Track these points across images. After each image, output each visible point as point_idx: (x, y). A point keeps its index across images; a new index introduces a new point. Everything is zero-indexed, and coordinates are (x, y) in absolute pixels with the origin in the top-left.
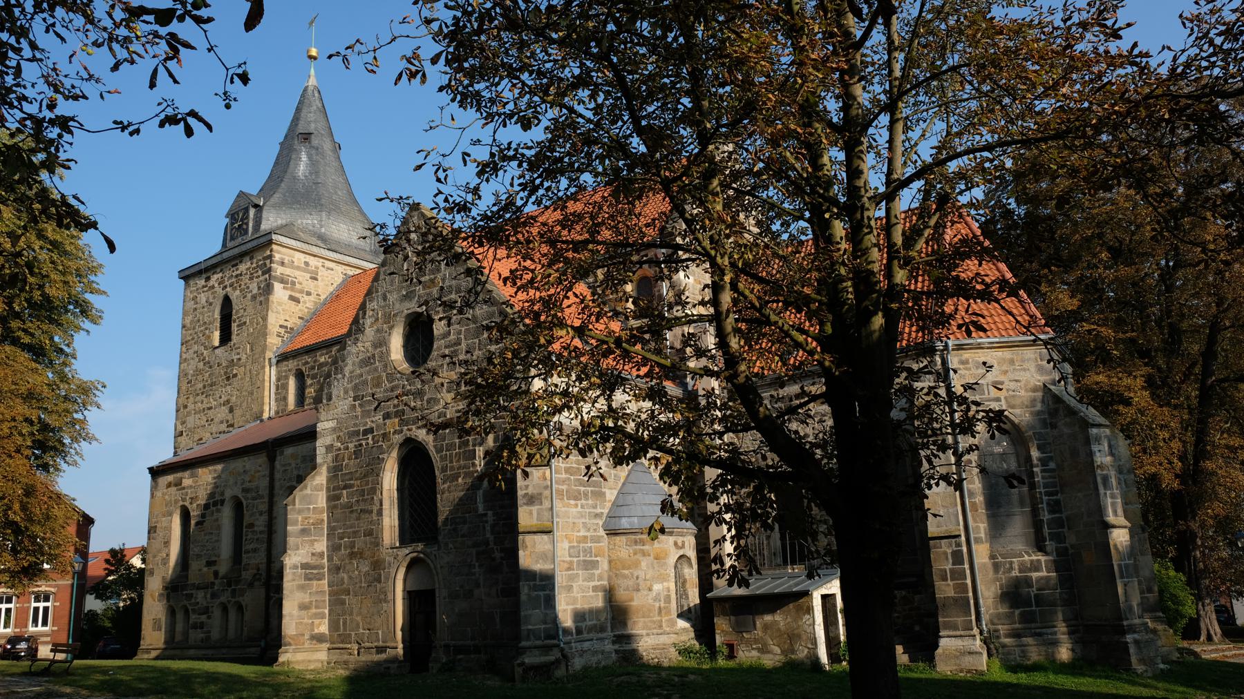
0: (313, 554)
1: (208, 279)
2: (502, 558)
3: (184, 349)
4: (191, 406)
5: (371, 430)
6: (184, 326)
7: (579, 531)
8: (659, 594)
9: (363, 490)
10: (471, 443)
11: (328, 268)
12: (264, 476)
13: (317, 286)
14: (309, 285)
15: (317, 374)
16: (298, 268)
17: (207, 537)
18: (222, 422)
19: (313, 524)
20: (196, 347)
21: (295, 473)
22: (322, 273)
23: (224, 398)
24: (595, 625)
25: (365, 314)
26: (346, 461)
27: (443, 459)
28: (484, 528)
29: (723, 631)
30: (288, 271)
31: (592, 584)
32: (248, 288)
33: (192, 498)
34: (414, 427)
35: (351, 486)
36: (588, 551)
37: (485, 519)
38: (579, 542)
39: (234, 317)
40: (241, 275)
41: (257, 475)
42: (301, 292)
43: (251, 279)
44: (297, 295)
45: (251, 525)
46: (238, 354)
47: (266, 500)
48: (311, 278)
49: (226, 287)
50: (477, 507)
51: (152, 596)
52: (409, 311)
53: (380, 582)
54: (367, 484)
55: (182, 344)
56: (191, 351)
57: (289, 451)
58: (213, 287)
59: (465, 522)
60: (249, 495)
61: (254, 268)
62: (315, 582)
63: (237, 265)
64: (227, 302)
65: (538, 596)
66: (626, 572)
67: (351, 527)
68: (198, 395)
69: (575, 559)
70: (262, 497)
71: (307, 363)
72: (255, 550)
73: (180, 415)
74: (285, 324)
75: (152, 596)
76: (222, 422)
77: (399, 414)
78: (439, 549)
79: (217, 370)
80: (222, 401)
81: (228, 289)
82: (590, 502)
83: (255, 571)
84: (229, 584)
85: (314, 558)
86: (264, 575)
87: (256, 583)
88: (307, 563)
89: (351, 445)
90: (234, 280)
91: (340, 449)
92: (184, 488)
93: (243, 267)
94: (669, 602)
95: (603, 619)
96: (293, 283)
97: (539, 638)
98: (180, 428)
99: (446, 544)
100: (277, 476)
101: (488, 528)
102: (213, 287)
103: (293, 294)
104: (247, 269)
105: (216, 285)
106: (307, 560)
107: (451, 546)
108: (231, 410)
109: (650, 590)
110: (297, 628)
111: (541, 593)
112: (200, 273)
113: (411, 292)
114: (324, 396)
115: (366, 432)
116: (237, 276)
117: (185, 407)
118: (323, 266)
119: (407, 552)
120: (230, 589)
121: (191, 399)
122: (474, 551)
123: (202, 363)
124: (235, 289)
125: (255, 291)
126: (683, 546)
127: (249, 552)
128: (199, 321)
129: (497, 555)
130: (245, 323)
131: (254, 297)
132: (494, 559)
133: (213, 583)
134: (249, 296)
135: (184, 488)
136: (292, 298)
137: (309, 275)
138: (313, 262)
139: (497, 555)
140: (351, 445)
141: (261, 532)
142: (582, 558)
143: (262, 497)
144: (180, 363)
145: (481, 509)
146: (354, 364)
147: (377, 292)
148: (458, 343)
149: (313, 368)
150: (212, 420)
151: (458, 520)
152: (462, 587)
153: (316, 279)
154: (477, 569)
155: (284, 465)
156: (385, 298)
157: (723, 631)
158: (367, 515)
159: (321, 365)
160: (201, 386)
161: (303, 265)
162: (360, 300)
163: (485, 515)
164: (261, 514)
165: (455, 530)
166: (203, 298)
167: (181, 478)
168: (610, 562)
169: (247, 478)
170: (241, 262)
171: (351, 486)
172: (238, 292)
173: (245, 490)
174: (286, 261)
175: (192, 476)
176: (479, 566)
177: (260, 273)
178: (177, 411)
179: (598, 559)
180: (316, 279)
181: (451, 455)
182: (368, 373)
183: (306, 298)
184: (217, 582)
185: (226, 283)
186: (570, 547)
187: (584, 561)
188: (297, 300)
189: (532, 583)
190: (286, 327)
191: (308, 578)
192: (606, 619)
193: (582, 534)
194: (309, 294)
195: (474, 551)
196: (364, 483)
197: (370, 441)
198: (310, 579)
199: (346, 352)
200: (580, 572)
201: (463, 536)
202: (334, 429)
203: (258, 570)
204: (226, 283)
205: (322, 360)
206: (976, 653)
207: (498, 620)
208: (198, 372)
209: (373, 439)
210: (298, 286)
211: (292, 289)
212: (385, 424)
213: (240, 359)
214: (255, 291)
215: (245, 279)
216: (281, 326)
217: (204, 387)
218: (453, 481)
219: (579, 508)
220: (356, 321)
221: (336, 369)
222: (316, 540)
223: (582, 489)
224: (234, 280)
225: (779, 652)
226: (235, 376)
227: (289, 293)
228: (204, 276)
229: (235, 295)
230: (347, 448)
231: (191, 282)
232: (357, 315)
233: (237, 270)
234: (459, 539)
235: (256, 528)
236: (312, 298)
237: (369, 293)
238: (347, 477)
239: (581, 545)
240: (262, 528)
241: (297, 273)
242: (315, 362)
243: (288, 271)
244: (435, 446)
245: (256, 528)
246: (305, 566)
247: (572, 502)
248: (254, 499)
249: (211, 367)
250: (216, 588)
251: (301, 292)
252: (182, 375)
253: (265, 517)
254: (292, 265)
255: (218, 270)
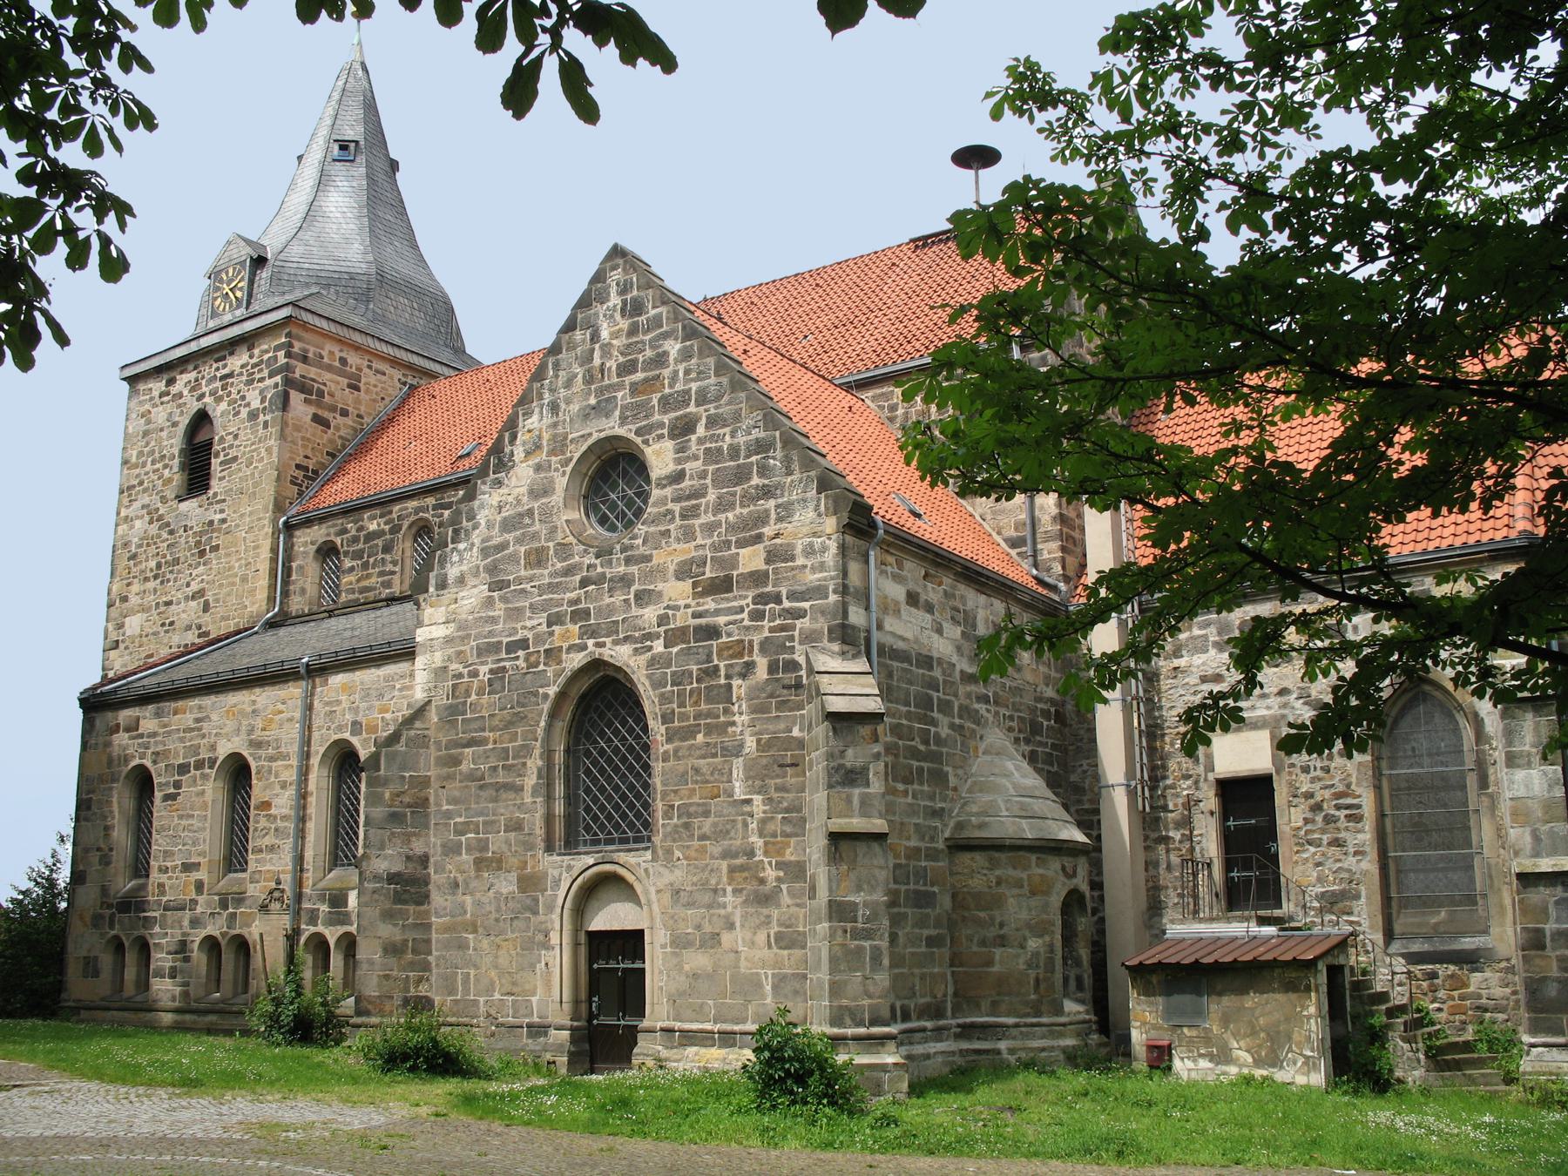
0: (408, 858)
1: (171, 382)
2: (778, 879)
3: (126, 501)
4: (134, 600)
5: (523, 644)
6: (125, 462)
7: (908, 839)
8: (1036, 954)
9: (506, 750)
10: (723, 673)
11: (377, 371)
12: (290, 720)
13: (358, 401)
14: (345, 397)
15: (362, 551)
16: (329, 368)
17: (184, 822)
18: (189, 628)
19: (409, 806)
20: (146, 500)
21: (349, 717)
22: (368, 378)
23: (195, 587)
24: (928, 1005)
25: (514, 438)
26: (474, 697)
27: (664, 699)
28: (745, 825)
29: (1144, 1023)
30: (312, 372)
31: (926, 932)
32: (243, 398)
33: (157, 754)
34: (608, 640)
35: (483, 742)
36: (921, 874)
37: (747, 809)
38: (908, 857)
39: (216, 447)
40: (231, 375)
41: (277, 718)
42: (333, 409)
43: (250, 382)
44: (326, 414)
45: (266, 805)
46: (222, 511)
47: (294, 762)
48: (350, 386)
49: (202, 396)
50: (733, 788)
51: (81, 918)
52: (603, 435)
53: (536, 913)
54: (514, 738)
55: (122, 492)
56: (137, 505)
57: (337, 680)
58: (180, 395)
59: (706, 814)
60: (261, 752)
61: (256, 365)
62: (411, 908)
63: (224, 358)
64: (202, 419)
65: (860, 949)
66: (982, 914)
67: (481, 814)
68: (146, 579)
69: (903, 888)
70: (286, 757)
71: (344, 531)
72: (272, 849)
73: (114, 612)
74: (305, 462)
75: (81, 918)
76: (189, 628)
77: (580, 615)
78: (653, 860)
79: (182, 538)
80: (189, 591)
81: (207, 399)
82: (926, 788)
83: (273, 885)
84: (224, 904)
85: (410, 865)
86: (289, 893)
87: (275, 906)
88: (398, 874)
89: (483, 669)
90: (218, 384)
91: (460, 676)
92: (141, 736)
93: (236, 362)
94: (1053, 971)
95: (939, 995)
96: (321, 394)
97: (860, 1024)
98: (113, 636)
99: (669, 852)
100: (318, 721)
101: (753, 826)
102: (180, 395)
103: (320, 412)
104: (242, 366)
105: (186, 393)
106: (398, 867)
107: (678, 854)
108: (206, 607)
109: (1022, 947)
110: (379, 985)
111: (867, 944)
112: (158, 371)
113: (607, 400)
114: (432, 582)
115: (512, 647)
116: (223, 378)
117: (125, 599)
118: (370, 367)
119: (591, 861)
120: (225, 914)
121: (135, 588)
122: (724, 865)
123: (156, 525)
124: (219, 400)
125: (256, 404)
126: (1074, 875)
127: (261, 851)
128: (153, 452)
129: (771, 874)
130: (235, 459)
131: (253, 416)
132: (762, 881)
133: (194, 902)
134: (244, 413)
135: (141, 736)
136: (317, 419)
137: (346, 381)
138: (354, 359)
139: (771, 874)
140: (483, 669)
141: (285, 818)
142: (912, 887)
143: (286, 757)
144: (117, 525)
145: (739, 792)
146: (490, 525)
147: (541, 397)
148: (699, 493)
149: (355, 540)
150: (172, 624)
151: (692, 809)
152: (698, 927)
153: (358, 389)
154: (729, 898)
155: (327, 704)
156: (554, 408)
157: (1144, 1023)
158: (512, 795)
159: (371, 536)
160: (153, 564)
161: (337, 364)
162: (507, 412)
163: (748, 802)
164: (284, 786)
165: (687, 826)
166: (160, 415)
167: (138, 719)
168: (954, 896)
169: (259, 723)
170: (232, 353)
171: (483, 742)
172: (223, 406)
173: (256, 745)
174: (310, 355)
175: (158, 715)
176: (735, 891)
177: (266, 373)
178: (110, 606)
179: (936, 889)
180: (358, 389)
181: (681, 694)
182: (519, 541)
183: (340, 420)
184: (201, 899)
185: (204, 389)
186: (896, 866)
187: (916, 892)
188: (325, 424)
189: (849, 925)
190: (306, 469)
191: (398, 898)
192: (945, 995)
193: (913, 843)
194: (344, 413)
195: (724, 865)
196: (507, 736)
197: (521, 663)
198: (405, 902)
199: (476, 503)
200: (909, 911)
201: (703, 838)
202: (449, 640)
203: (279, 883)
204: (204, 389)
205: (373, 526)
206: (218, 981)
207: (769, 988)
208: (148, 541)
209: (526, 660)
210: (327, 398)
211: (319, 404)
212: (551, 634)
213: (224, 521)
214: (256, 404)
215: (237, 384)
216: (298, 467)
217: (159, 566)
218: (684, 739)
219: (910, 800)
220: (497, 449)
221: (456, 532)
222: (414, 834)
223: (915, 764)
224: (218, 384)
225: (1250, 1060)
226: (216, 548)
227: (312, 410)
228: (166, 377)
229: (218, 411)
230: (474, 674)
231: (141, 387)
232: (500, 440)
233: (225, 366)
234: (696, 843)
235: (273, 811)
236: (349, 421)
237: (524, 400)
238: (474, 725)
239: (912, 863)
240: (285, 811)
241: (327, 376)
242: (360, 529)
243: (312, 372)
244: (649, 677)
245: (273, 811)
246: (393, 878)
247: (901, 787)
248: (272, 759)
249: (171, 532)
250: (199, 909)
251: (333, 409)
252: (120, 547)
253: (291, 792)
254: (318, 362)
255: (191, 367)
